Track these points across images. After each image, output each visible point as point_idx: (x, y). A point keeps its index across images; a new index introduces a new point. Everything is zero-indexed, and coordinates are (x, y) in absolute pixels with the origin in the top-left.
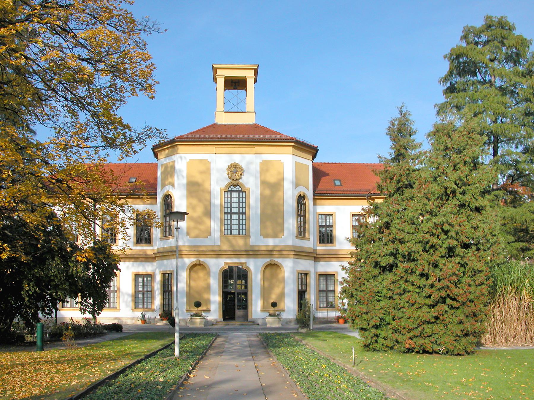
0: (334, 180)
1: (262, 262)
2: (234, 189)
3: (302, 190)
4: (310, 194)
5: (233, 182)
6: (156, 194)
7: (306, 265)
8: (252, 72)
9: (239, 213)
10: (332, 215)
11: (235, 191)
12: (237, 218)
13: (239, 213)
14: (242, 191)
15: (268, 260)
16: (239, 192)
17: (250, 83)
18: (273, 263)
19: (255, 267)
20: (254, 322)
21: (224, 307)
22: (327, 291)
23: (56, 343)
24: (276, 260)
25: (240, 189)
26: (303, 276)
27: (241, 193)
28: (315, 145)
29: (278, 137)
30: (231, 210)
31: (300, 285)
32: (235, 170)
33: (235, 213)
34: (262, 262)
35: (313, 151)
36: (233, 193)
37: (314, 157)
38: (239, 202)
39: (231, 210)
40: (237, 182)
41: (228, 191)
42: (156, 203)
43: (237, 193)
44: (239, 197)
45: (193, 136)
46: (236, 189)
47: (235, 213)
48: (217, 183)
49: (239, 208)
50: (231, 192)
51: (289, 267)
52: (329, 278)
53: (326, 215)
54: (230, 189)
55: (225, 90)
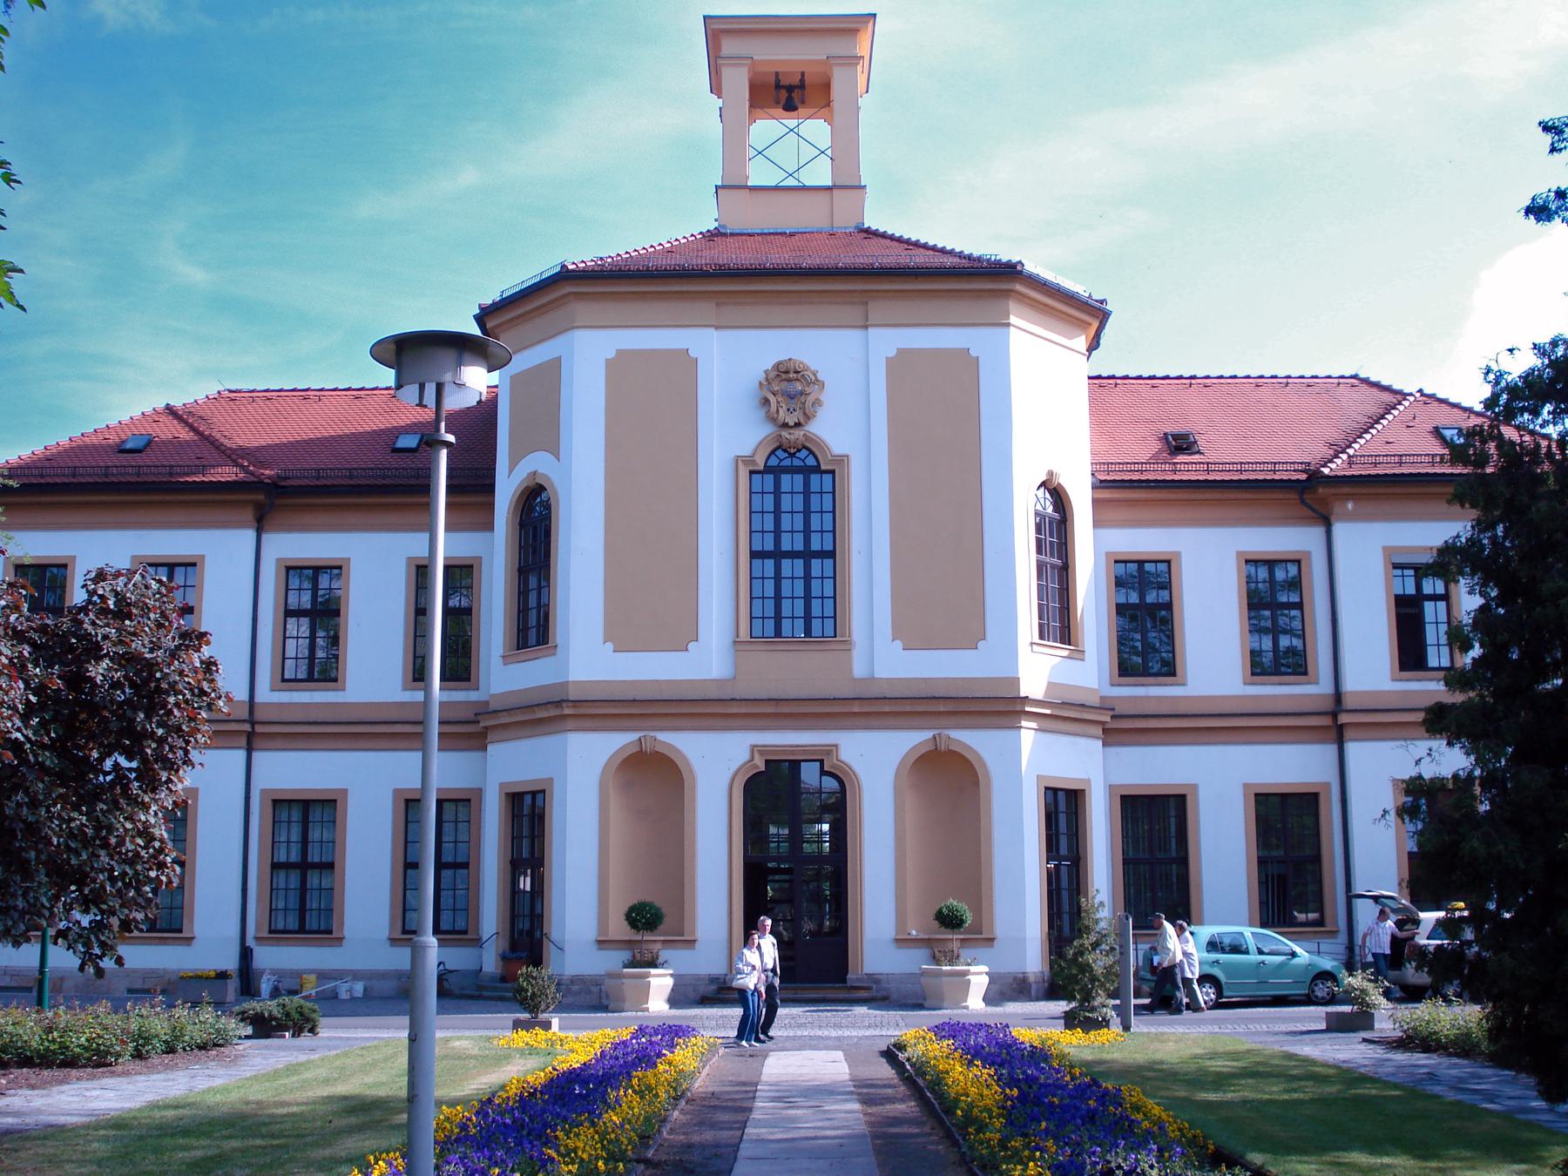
2: (787, 462)
6: (490, 489)
11: (792, 470)
12: (799, 572)
14: (817, 469)
19: (875, 761)
22: (304, 866)
23: (88, 1119)
25: (811, 461)
27: (815, 478)
29: (949, 261)
30: (807, 541)
32: (789, 388)
33: (793, 555)
34: (900, 743)
39: (807, 541)
40: (798, 434)
42: (489, 526)
43: (799, 478)
46: (797, 462)
47: (793, 555)
48: (728, 433)
53: (171, 567)
54: (773, 462)
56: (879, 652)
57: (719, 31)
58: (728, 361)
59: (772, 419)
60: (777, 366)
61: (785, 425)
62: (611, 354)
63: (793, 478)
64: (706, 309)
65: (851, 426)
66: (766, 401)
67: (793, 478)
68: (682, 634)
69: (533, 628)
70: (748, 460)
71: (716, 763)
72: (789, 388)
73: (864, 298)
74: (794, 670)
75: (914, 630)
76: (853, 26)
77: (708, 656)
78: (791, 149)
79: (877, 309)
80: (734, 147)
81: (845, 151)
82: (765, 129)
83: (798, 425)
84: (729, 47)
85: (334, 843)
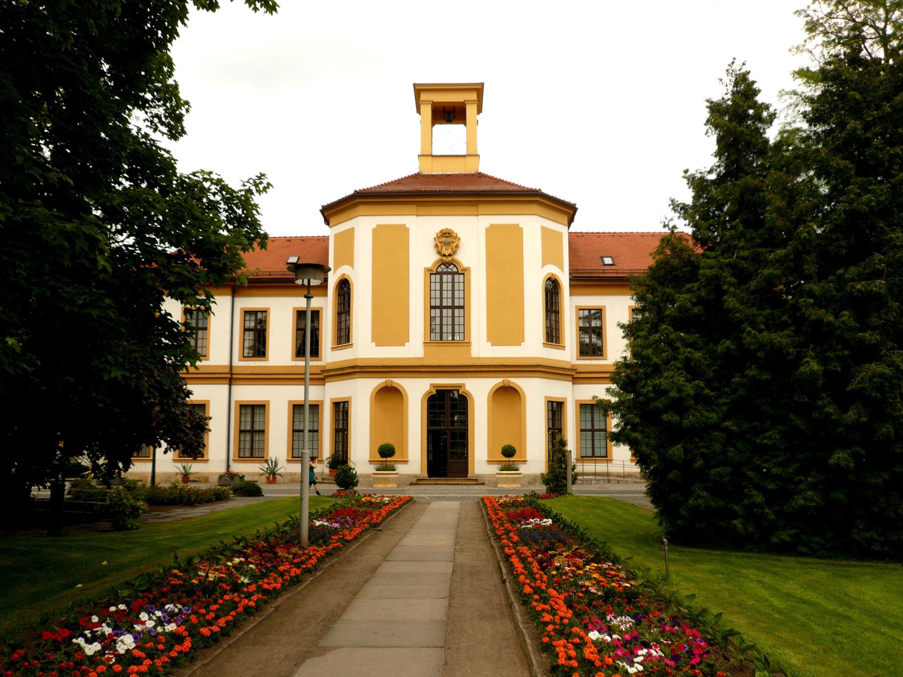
0: (602, 258)
1: (492, 383)
2: (445, 270)
3: (552, 269)
4: (564, 280)
5: (444, 259)
7: (561, 390)
9: (453, 307)
10: (266, 311)
11: (447, 273)
13: (453, 307)
14: (457, 273)
15: (501, 380)
16: (453, 274)
18: (507, 385)
19: (479, 391)
20: (477, 480)
21: (431, 455)
22: (253, 432)
25: (455, 270)
26: (555, 409)
27: (456, 277)
28: (572, 202)
30: (453, 302)
31: (341, 422)
32: (447, 239)
34: (492, 383)
35: (568, 211)
36: (445, 277)
37: (571, 220)
38: (453, 290)
39: (453, 302)
40: (450, 259)
41: (437, 273)
43: (450, 276)
44: (453, 282)
45: (390, 189)
47: (447, 307)
48: (422, 256)
49: (453, 298)
50: (441, 274)
51: (536, 393)
52: (257, 411)
54: (440, 270)
56: (482, 348)
57: (419, 90)
58: (422, 229)
59: (439, 253)
60: (441, 231)
61: (444, 255)
64: (413, 208)
65: (472, 254)
66: (437, 246)
67: (447, 268)
69: (343, 336)
70: (429, 270)
71: (416, 391)
72: (447, 239)
73: (476, 204)
75: (495, 338)
76: (478, 89)
77: (414, 349)
78: (449, 138)
79: (482, 208)
80: (428, 139)
81: (471, 140)
82: (442, 129)
83: (450, 255)
84: (424, 96)
85: (265, 421)
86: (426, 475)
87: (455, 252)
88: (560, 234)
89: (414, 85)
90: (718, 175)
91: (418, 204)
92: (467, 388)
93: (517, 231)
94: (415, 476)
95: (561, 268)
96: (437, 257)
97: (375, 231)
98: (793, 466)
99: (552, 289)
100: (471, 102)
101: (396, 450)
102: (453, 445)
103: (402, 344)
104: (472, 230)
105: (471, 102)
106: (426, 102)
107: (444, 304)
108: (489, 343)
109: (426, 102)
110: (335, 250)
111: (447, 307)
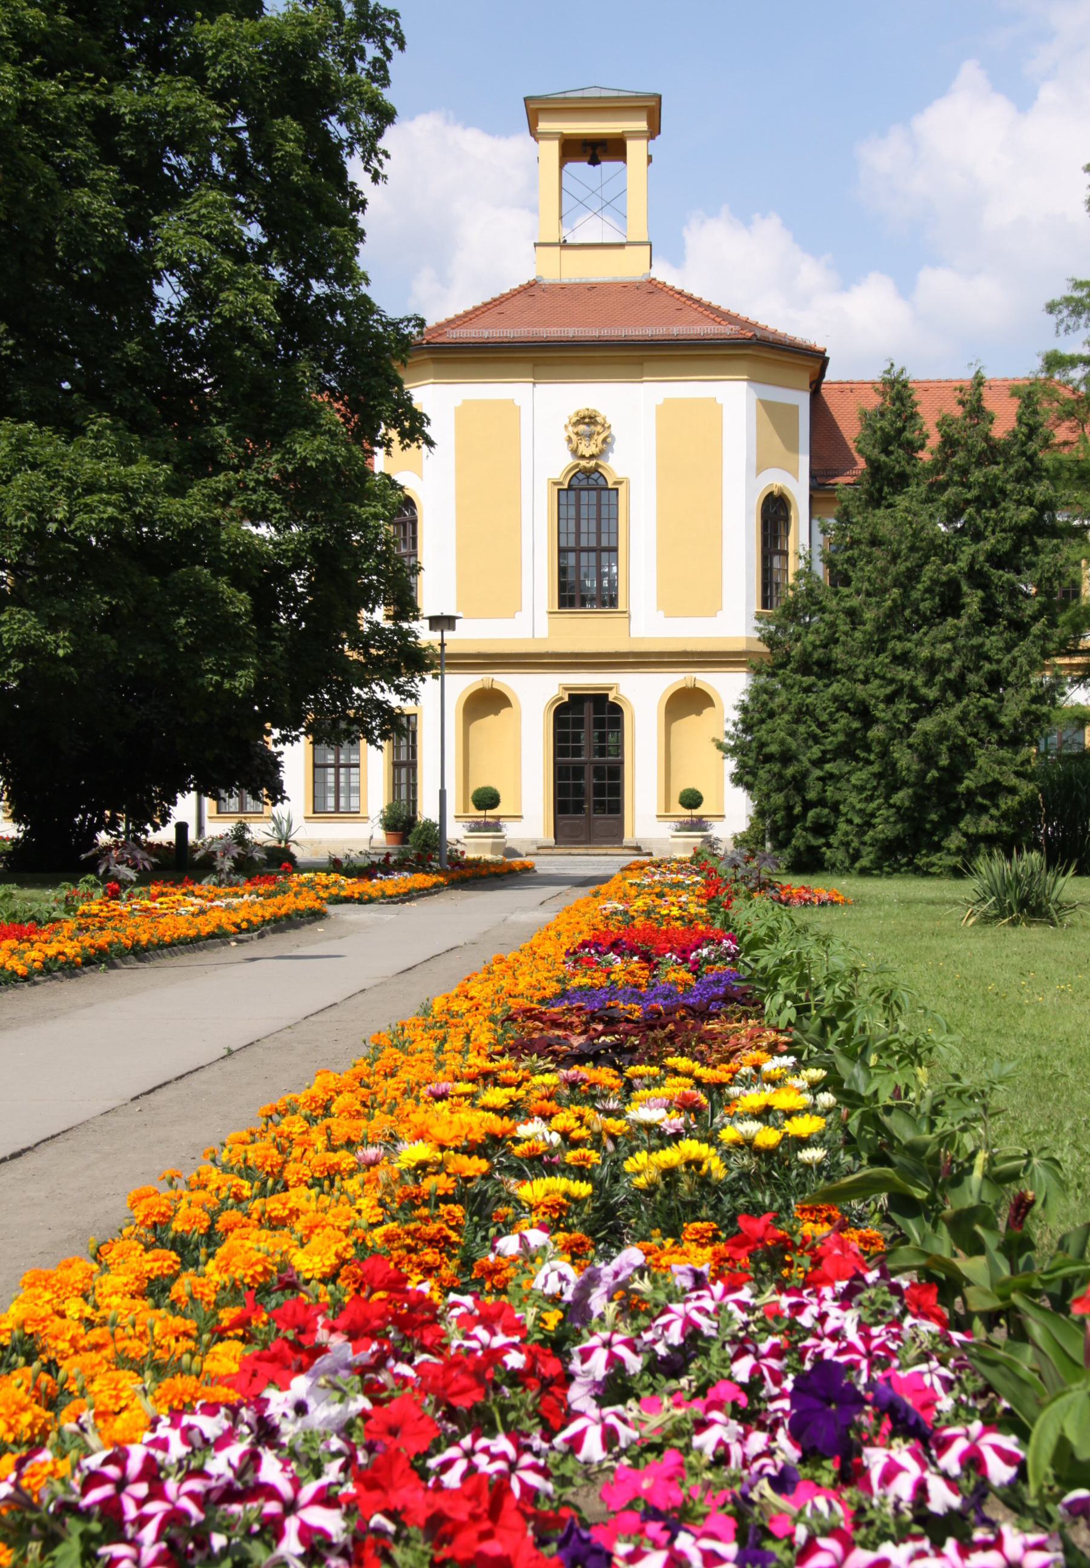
8: (642, 125)
15: (479, 677)
17: (636, 149)
19: (642, 696)
24: (497, 677)
28: (820, 346)
40: (593, 463)
47: (589, 550)
48: (551, 461)
55: (562, 164)
58: (543, 411)
59: (574, 452)
61: (583, 457)
62: (459, 403)
63: (587, 498)
65: (630, 464)
66: (570, 440)
67: (587, 498)
68: (712, 606)
71: (535, 696)
73: (639, 362)
74: (588, 632)
83: (592, 457)
86: (551, 840)
87: (602, 452)
88: (795, 409)
89: (525, 99)
90: (149, 810)
91: (536, 363)
92: (621, 692)
93: (713, 408)
94: (534, 842)
95: (795, 474)
96: (568, 460)
97: (459, 412)
98: (254, 530)
99: (774, 512)
100: (636, 135)
101: (502, 798)
102: (599, 790)
103: (668, 402)
104: (634, 409)
105: (636, 135)
106: (548, 136)
107: (584, 543)
108: (661, 613)
109: (548, 136)
110: (462, 552)
111: (589, 550)
